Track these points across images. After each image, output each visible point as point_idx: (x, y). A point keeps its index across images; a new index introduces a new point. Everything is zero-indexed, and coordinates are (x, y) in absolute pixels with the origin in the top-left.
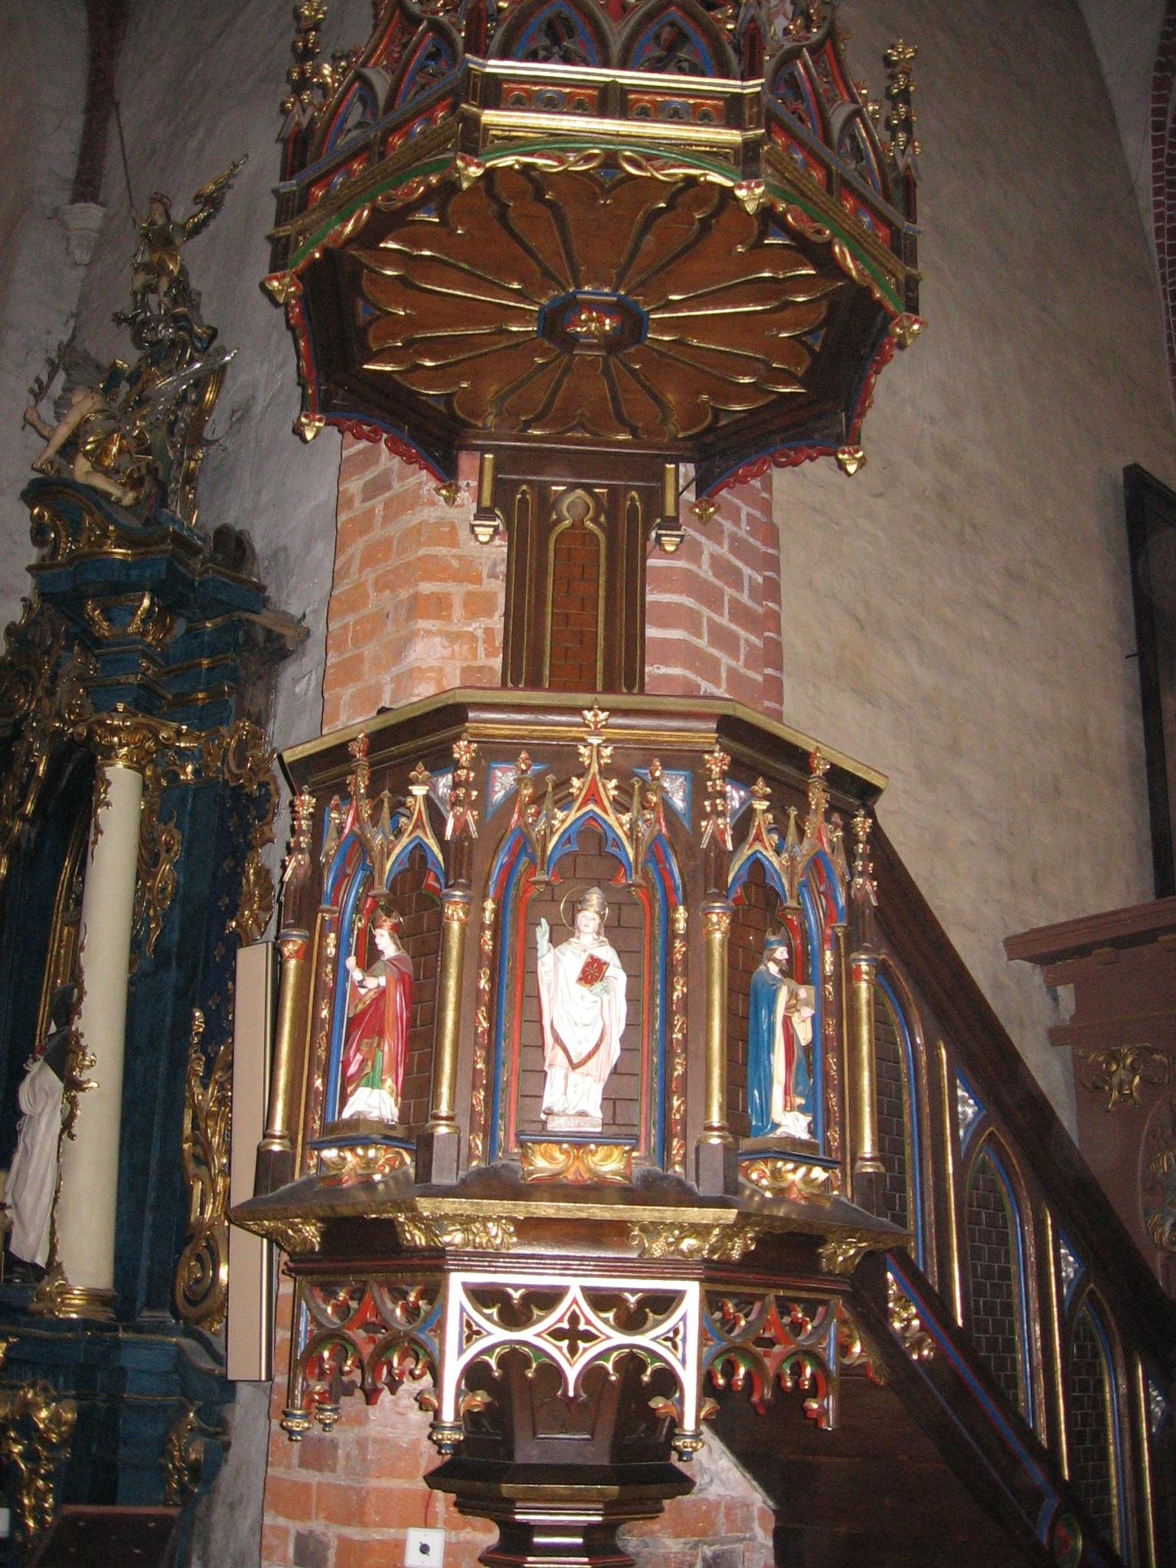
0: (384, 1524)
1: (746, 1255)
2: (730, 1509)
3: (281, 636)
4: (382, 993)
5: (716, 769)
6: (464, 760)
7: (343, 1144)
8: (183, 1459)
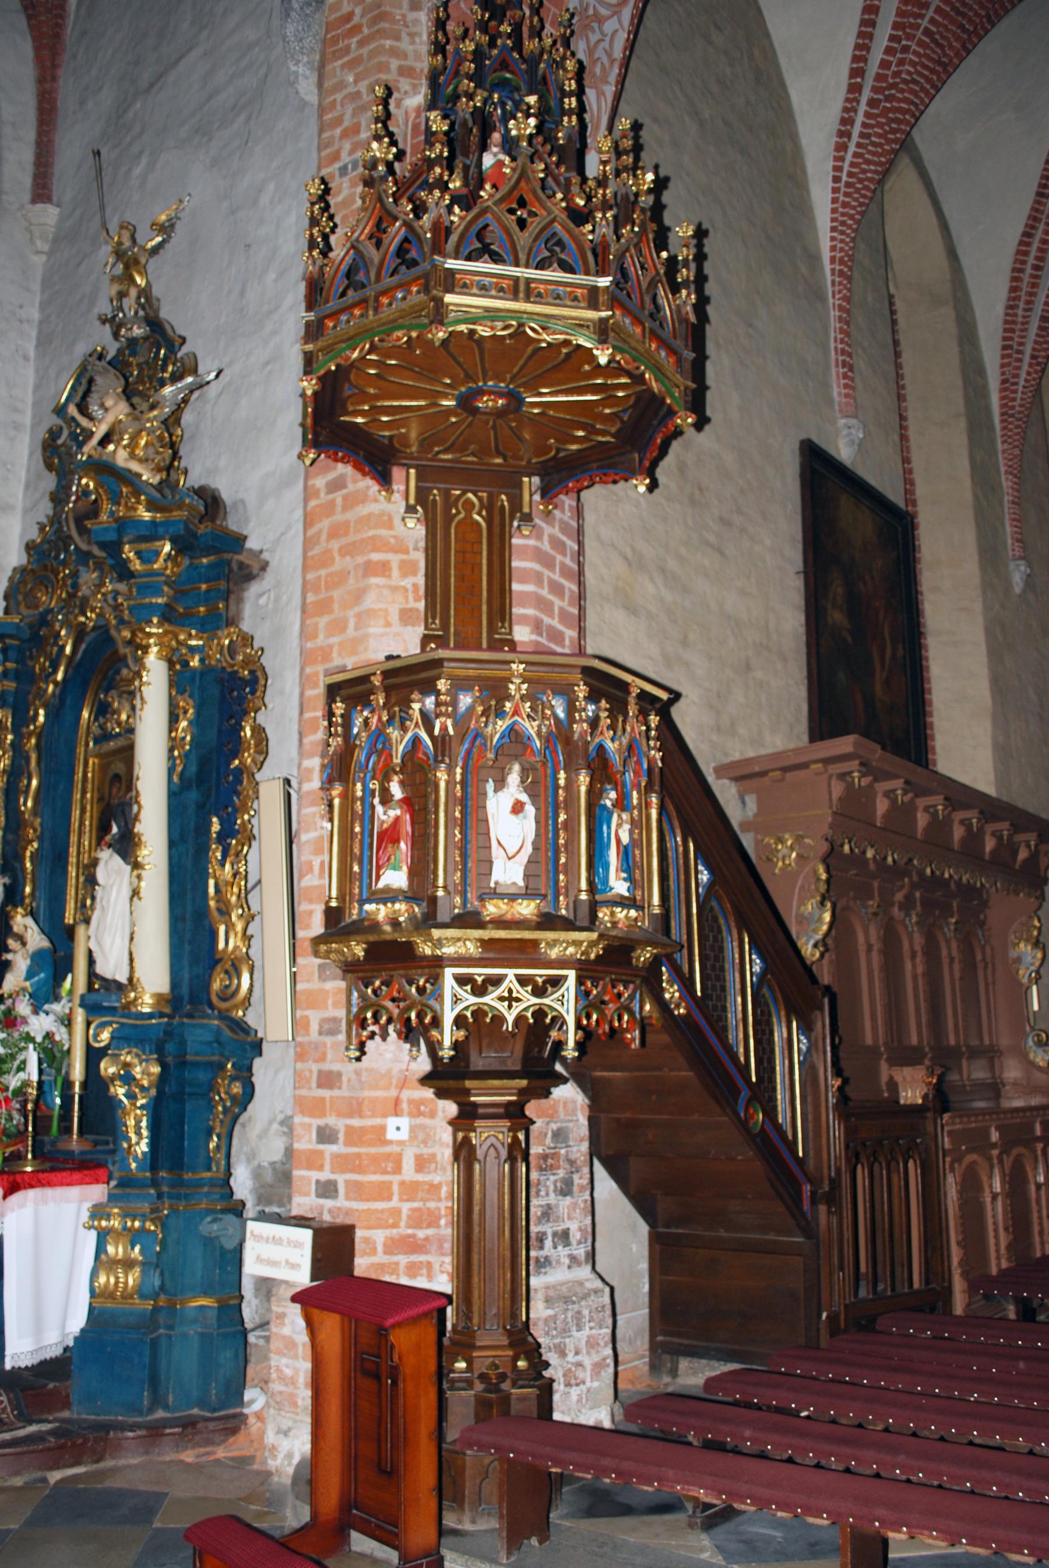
0: (373, 1116)
1: (598, 956)
2: (565, 1103)
3: (248, 566)
4: (397, 819)
5: (581, 695)
6: (443, 690)
7: (378, 901)
8: (227, 1093)
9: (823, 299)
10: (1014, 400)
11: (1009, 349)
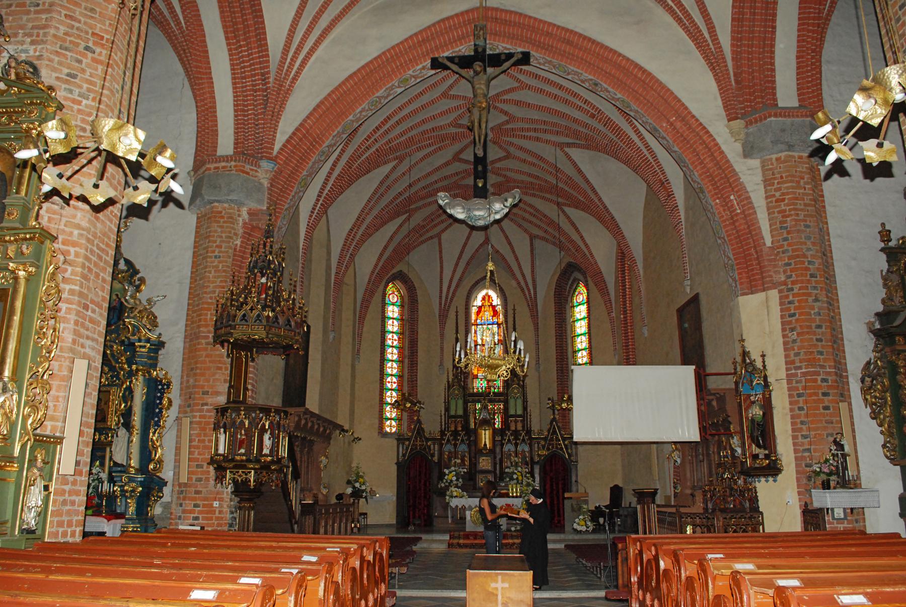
9: (298, 261)
10: (269, 83)
11: (340, 263)
